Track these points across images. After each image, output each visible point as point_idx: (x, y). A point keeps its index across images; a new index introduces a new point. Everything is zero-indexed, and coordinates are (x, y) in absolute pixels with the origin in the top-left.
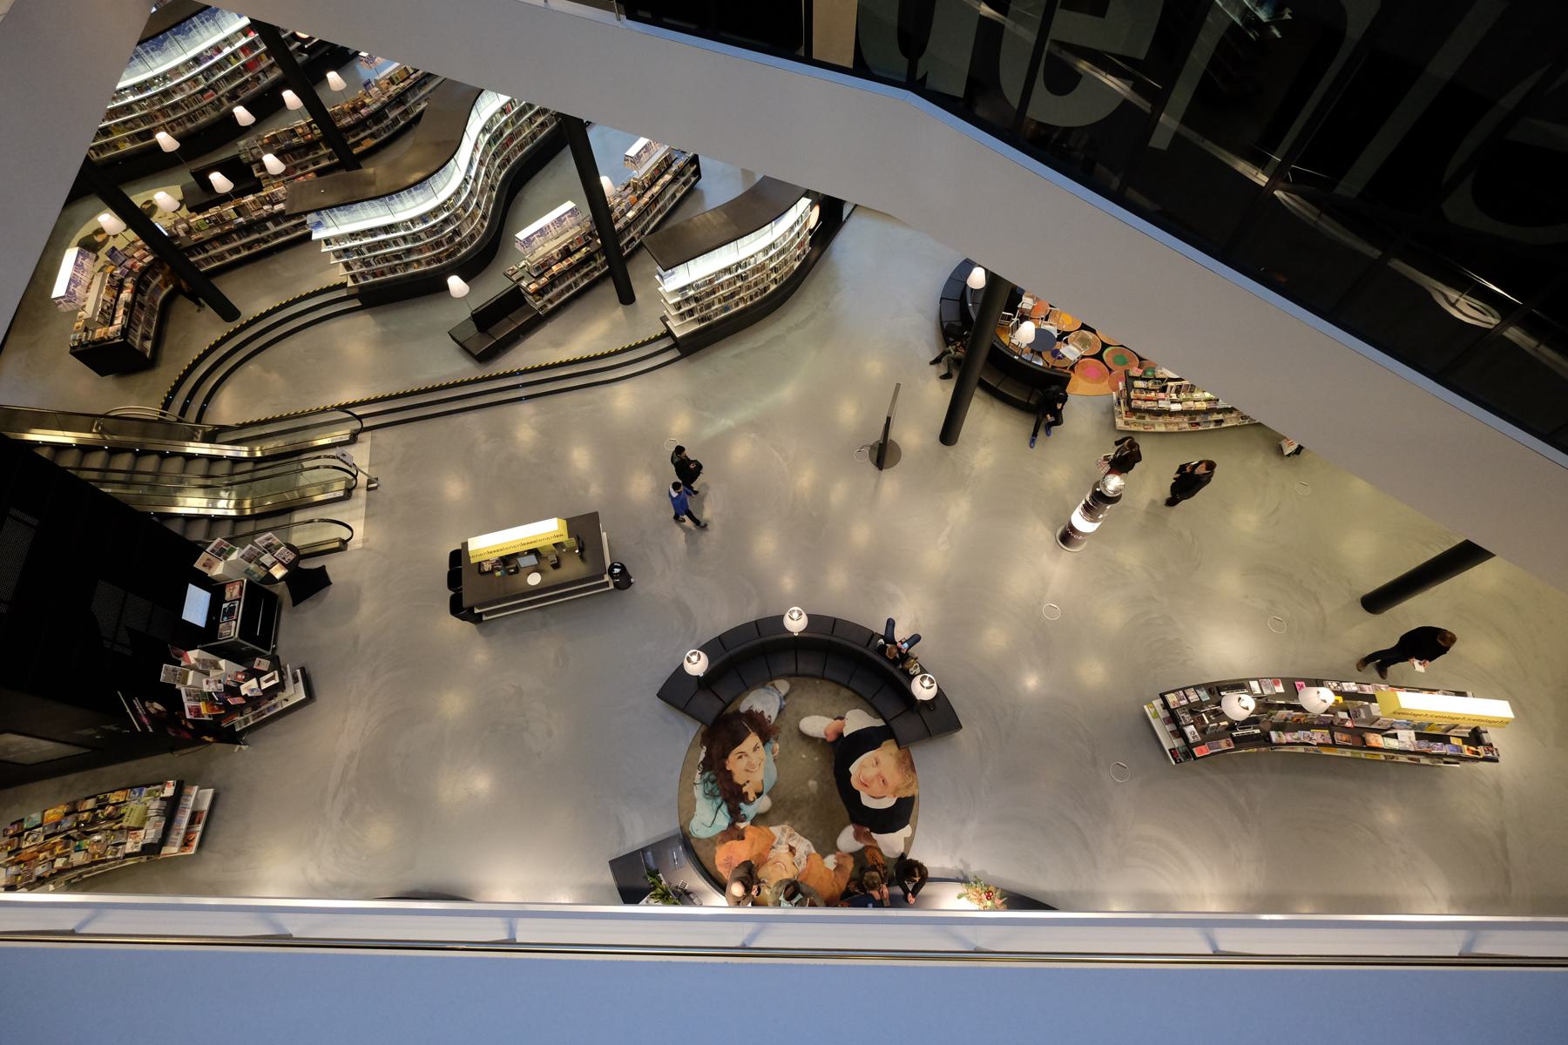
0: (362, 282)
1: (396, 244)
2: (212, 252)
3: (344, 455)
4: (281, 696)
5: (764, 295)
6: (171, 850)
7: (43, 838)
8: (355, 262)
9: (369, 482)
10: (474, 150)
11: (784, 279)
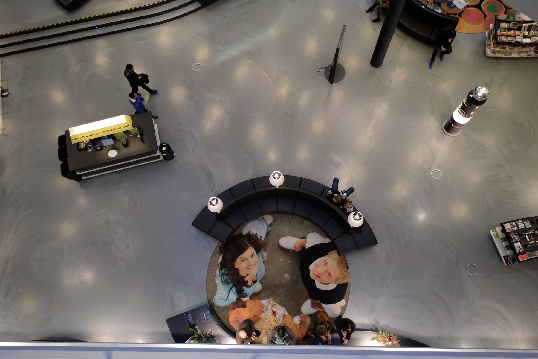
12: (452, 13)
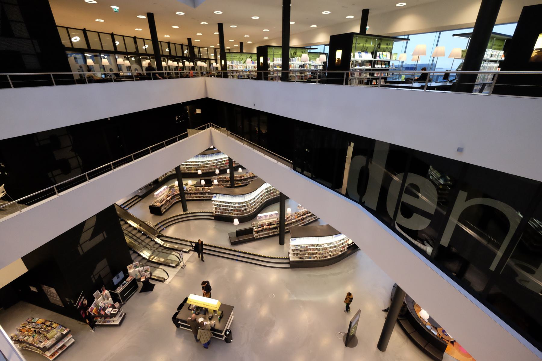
0: (217, 213)
1: (229, 207)
2: (192, 196)
3: (181, 254)
4: (114, 319)
5: (325, 259)
6: (48, 354)
7: (32, 327)
8: (218, 208)
9: (183, 266)
10: (261, 192)
11: (334, 256)
12: (446, 339)
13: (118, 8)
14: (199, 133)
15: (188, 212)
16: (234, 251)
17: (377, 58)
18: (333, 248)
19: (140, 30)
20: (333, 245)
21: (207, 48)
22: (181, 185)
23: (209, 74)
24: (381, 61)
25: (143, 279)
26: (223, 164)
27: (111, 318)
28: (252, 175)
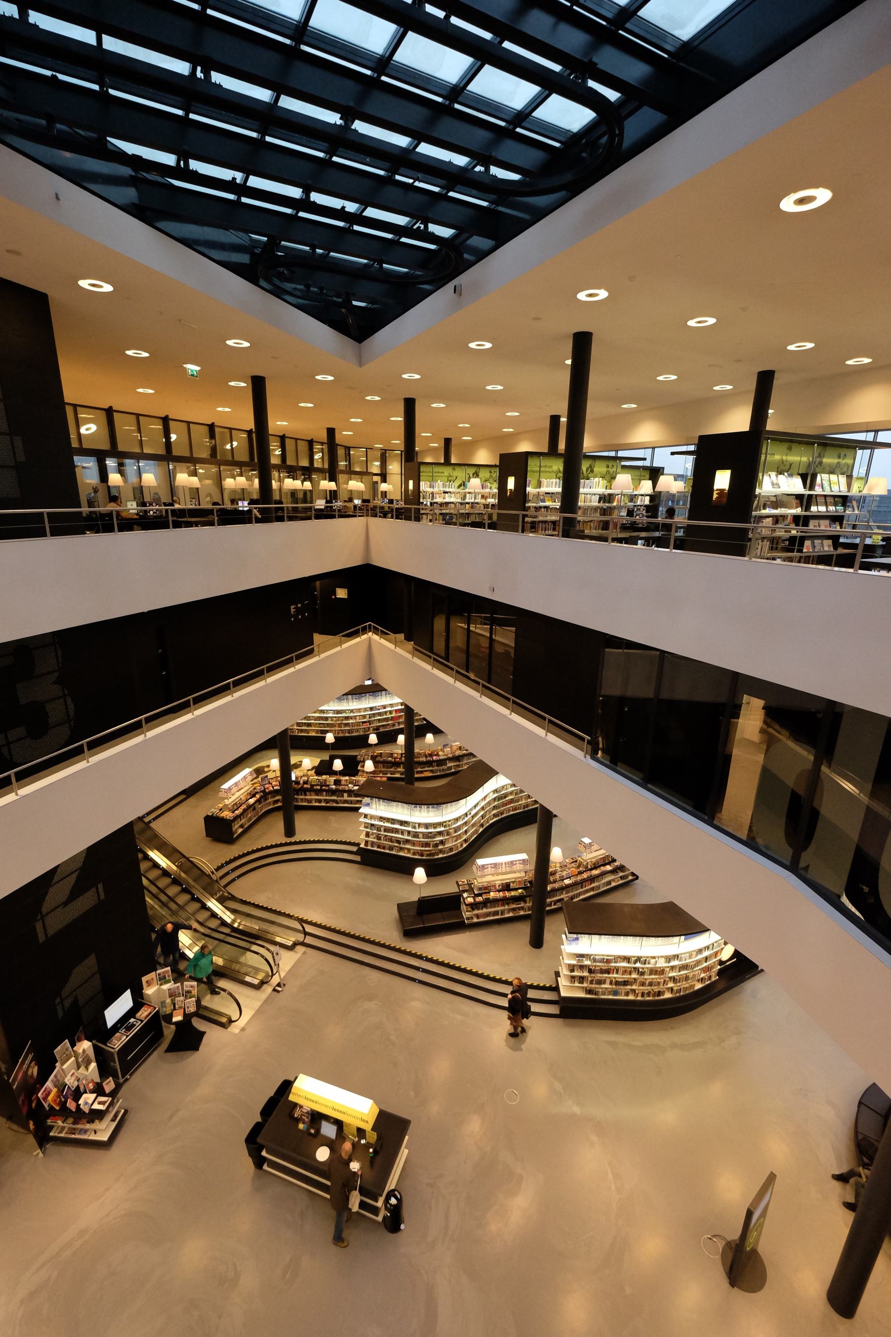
0: (369, 848)
1: (402, 833)
3: (277, 954)
4: (97, 1125)
8: (373, 834)
9: (279, 985)
10: (482, 800)
11: (682, 994)
13: (198, 368)
14: (344, 646)
15: (296, 838)
16: (410, 954)
17: (817, 488)
18: (679, 971)
19: (228, 410)
20: (681, 963)
21: (366, 449)
22: (286, 769)
23: (369, 509)
24: (825, 496)
25: (177, 1018)
26: (387, 719)
27: (91, 1121)
28: (458, 753)
